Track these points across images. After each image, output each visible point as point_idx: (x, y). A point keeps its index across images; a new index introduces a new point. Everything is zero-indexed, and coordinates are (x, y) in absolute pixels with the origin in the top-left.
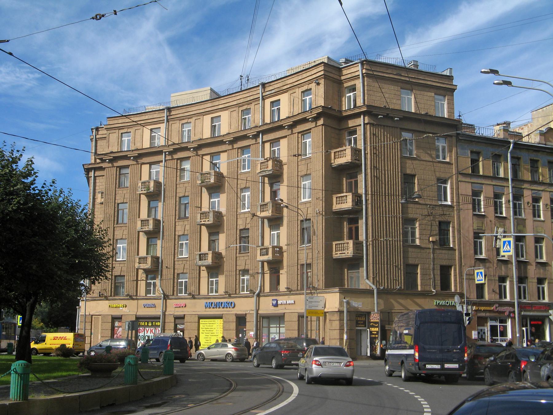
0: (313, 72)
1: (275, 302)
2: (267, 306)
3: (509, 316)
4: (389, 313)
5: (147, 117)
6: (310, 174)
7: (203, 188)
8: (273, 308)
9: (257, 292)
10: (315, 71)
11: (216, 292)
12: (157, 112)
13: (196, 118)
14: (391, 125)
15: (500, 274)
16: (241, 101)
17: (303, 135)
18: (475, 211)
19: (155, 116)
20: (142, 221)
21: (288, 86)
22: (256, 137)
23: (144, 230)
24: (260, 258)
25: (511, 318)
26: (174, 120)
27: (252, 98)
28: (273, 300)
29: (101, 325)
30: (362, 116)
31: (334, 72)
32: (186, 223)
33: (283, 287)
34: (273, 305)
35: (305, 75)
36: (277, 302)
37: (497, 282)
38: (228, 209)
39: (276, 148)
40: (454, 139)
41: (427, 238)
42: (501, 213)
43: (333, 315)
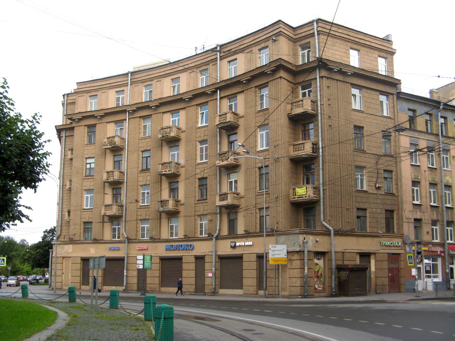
0: (269, 31)
1: (233, 244)
2: (225, 248)
3: (440, 256)
4: (343, 252)
5: (112, 81)
6: (267, 124)
7: (163, 142)
8: (231, 250)
9: (216, 235)
10: (272, 29)
11: (176, 234)
12: (121, 77)
13: (157, 80)
14: (342, 80)
15: (433, 219)
16: (199, 62)
17: (260, 89)
18: (413, 162)
19: (119, 80)
20: (107, 172)
21: (245, 45)
22: (214, 92)
23: (109, 180)
24: (219, 203)
25: (442, 256)
26: (138, 83)
27: (209, 59)
28: (231, 242)
29: (72, 266)
30: (318, 71)
31: (289, 30)
32: (148, 174)
33: (240, 230)
34: (231, 247)
35: (261, 35)
36: (235, 244)
37: (430, 225)
38: (186, 160)
39: (233, 103)
40: (395, 97)
41: (374, 185)
42: (433, 165)
43: (293, 255)
